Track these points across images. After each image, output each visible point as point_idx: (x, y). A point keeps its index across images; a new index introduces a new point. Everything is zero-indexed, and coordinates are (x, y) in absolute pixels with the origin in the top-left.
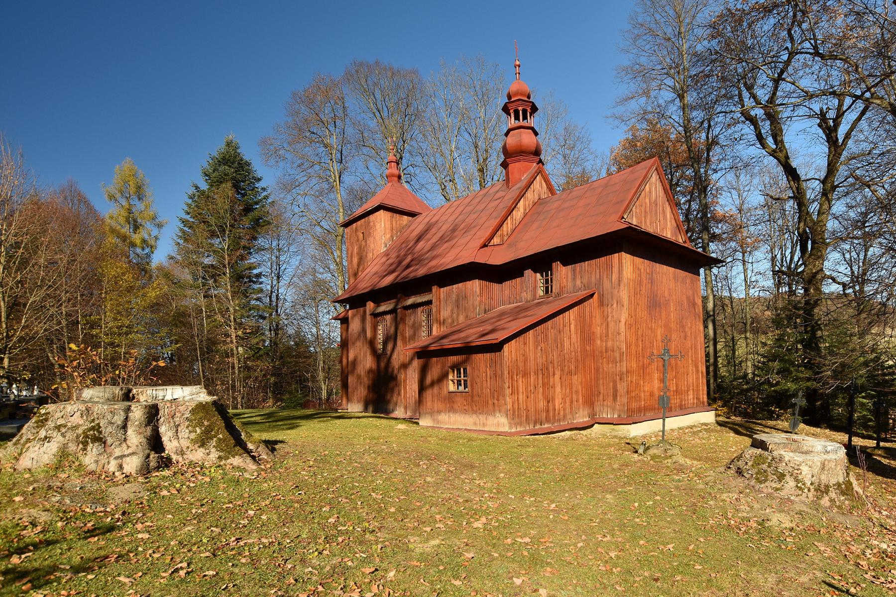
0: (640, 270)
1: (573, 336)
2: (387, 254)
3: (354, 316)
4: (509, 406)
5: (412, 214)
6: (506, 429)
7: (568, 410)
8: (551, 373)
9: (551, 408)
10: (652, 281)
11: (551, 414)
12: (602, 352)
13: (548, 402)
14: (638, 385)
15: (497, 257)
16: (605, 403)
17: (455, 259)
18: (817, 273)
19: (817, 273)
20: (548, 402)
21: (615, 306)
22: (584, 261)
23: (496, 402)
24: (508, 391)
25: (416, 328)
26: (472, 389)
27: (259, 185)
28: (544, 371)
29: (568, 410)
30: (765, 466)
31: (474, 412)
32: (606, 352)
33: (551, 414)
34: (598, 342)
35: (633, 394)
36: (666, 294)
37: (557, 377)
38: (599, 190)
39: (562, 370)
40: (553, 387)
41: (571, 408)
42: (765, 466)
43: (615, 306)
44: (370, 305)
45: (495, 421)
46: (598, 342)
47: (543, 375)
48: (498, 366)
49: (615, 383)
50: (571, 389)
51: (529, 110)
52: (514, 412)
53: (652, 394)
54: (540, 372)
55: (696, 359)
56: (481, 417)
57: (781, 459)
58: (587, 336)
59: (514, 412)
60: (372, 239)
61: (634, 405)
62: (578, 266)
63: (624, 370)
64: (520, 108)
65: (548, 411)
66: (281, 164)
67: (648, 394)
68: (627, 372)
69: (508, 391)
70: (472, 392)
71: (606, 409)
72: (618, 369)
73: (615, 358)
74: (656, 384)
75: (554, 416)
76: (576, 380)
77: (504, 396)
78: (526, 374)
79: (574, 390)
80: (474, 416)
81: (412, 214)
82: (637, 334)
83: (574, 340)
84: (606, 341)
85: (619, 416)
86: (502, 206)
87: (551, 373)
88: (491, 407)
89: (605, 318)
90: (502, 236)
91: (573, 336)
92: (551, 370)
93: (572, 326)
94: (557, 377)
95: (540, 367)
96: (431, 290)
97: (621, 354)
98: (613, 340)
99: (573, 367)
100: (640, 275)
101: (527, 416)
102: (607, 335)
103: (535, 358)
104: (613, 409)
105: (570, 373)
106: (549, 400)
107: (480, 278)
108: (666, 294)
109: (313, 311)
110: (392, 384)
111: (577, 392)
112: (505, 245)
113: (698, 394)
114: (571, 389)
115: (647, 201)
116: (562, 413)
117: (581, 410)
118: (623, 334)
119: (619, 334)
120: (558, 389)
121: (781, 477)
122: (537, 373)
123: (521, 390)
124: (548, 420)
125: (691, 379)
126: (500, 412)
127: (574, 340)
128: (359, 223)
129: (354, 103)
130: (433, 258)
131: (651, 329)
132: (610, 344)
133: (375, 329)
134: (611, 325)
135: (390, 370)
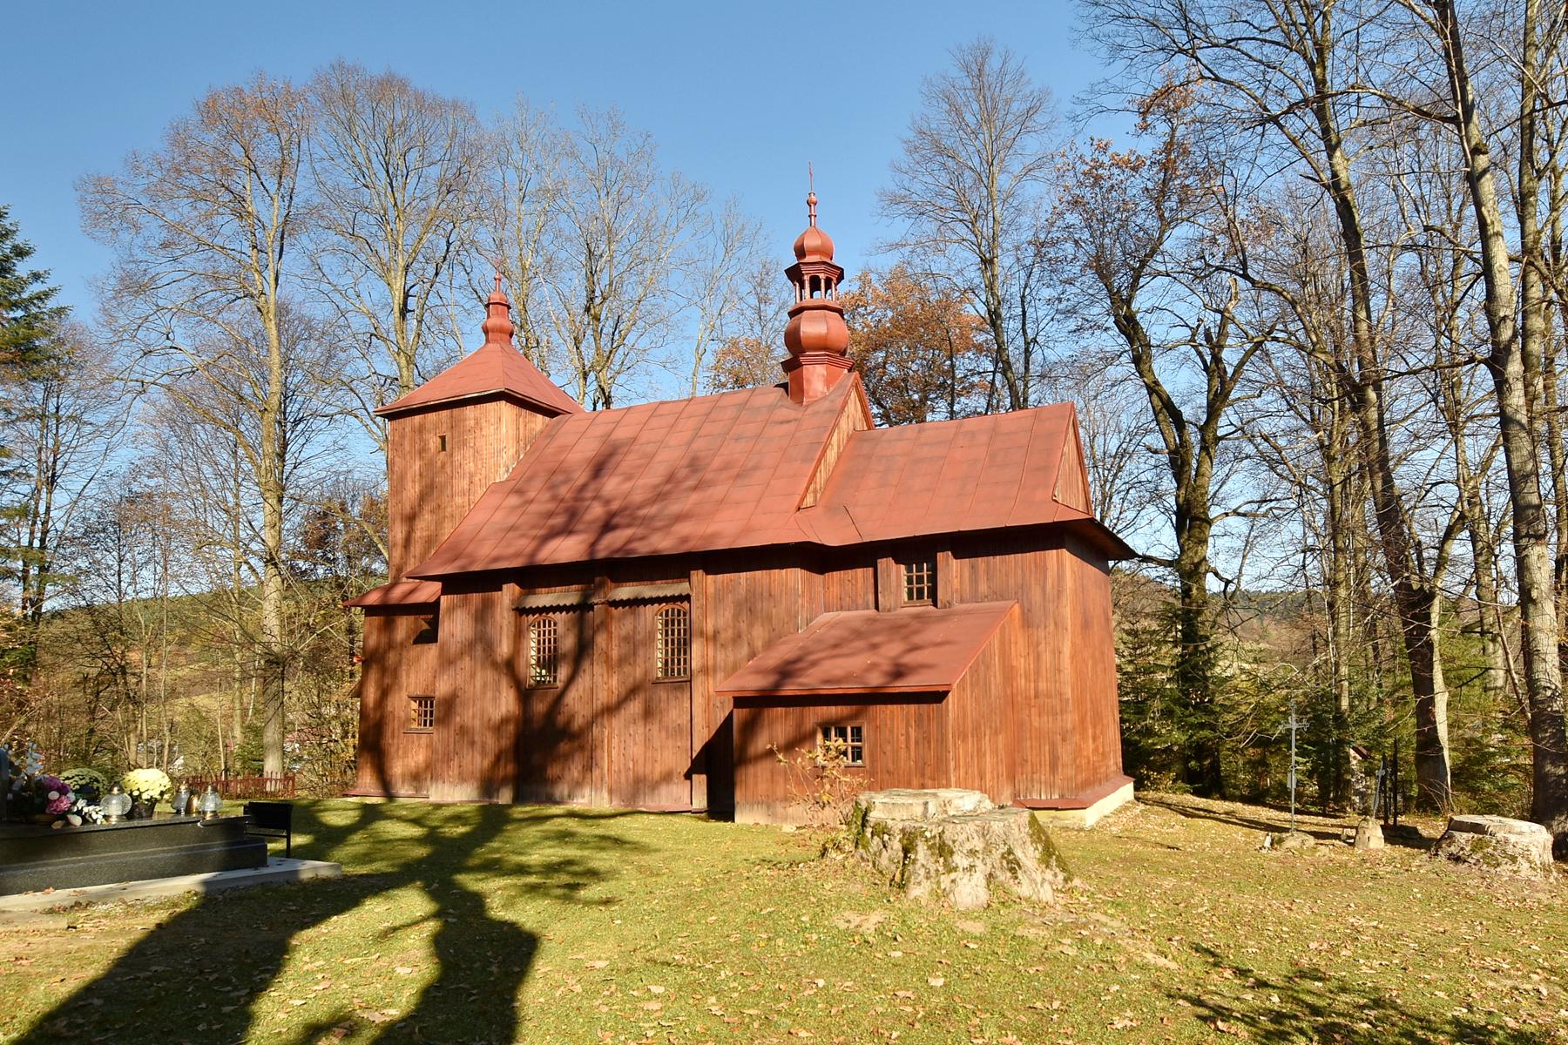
2: (517, 488)
3: (452, 609)
5: (551, 413)
15: (833, 536)
17: (747, 531)
18: (1200, 563)
19: (1200, 563)
22: (994, 554)
25: (635, 645)
26: (873, 761)
27: (22, 268)
30: (1490, 850)
32: (1036, 696)
42: (1490, 850)
43: (1052, 627)
48: (934, 725)
49: (1053, 745)
57: (1506, 841)
60: (469, 453)
62: (981, 562)
64: (822, 276)
66: (126, 237)
70: (872, 766)
71: (1037, 786)
81: (551, 413)
84: (1036, 681)
85: (1062, 796)
89: (1033, 645)
90: (815, 492)
96: (688, 577)
102: (1037, 673)
104: (1051, 786)
107: (802, 567)
109: (111, 559)
110: (564, 747)
121: (1513, 859)
128: (432, 416)
129: (321, 139)
130: (680, 518)
133: (519, 636)
135: (561, 719)
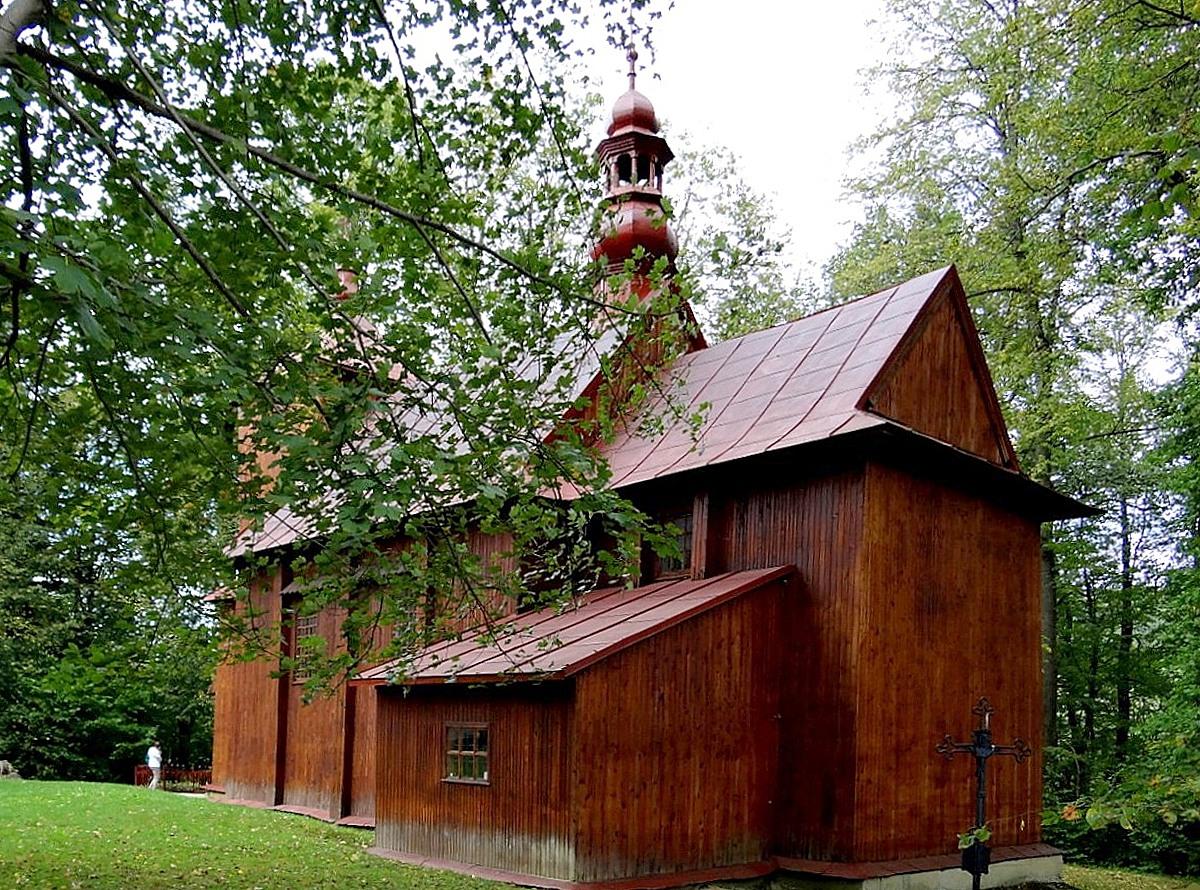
4: (582, 825)
36: (960, 583)
37: (696, 759)
39: (707, 748)
41: (723, 836)
51: (633, 154)
53: (914, 812)
65: (669, 839)
74: (926, 789)
93: (736, 649)
94: (696, 759)
100: (901, 537)
106: (675, 814)
108: (960, 583)
115: (926, 365)
131: (921, 662)
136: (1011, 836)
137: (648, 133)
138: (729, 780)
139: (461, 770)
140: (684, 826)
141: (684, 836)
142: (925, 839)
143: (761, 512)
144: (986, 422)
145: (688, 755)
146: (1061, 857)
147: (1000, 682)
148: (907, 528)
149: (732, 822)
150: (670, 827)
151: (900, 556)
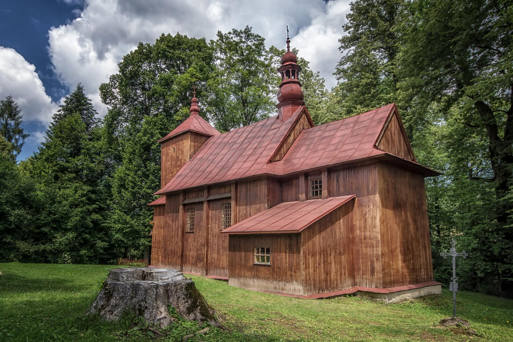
0: (387, 181)
1: (342, 227)
4: (304, 278)
6: (302, 293)
7: (339, 281)
8: (329, 254)
9: (329, 279)
10: (395, 189)
11: (329, 284)
12: (361, 239)
13: (327, 274)
14: (389, 264)
16: (365, 276)
20: (327, 274)
21: (371, 207)
23: (293, 273)
24: (302, 267)
28: (324, 252)
29: (339, 281)
31: (274, 279)
33: (329, 284)
34: (358, 232)
35: (386, 271)
36: (404, 198)
37: (332, 256)
38: (352, 125)
39: (335, 252)
40: (330, 264)
41: (341, 280)
43: (371, 207)
44: (181, 198)
45: (292, 287)
46: (358, 232)
47: (324, 255)
49: (372, 262)
50: (341, 265)
52: (306, 282)
54: (322, 253)
55: (425, 244)
56: (280, 283)
58: (351, 229)
59: (306, 282)
61: (388, 279)
63: (380, 253)
65: (327, 281)
67: (395, 271)
68: (382, 255)
69: (302, 267)
72: (375, 252)
73: (372, 244)
75: (331, 285)
76: (344, 258)
77: (300, 270)
78: (314, 255)
79: (343, 266)
80: (275, 282)
82: (387, 228)
83: (342, 230)
84: (365, 232)
86: (278, 134)
87: (329, 254)
88: (289, 277)
91: (342, 227)
92: (329, 251)
94: (332, 256)
95: (322, 249)
97: (377, 242)
98: (370, 231)
99: (342, 249)
100: (388, 185)
101: (314, 285)
102: (365, 227)
103: (320, 243)
104: (371, 281)
105: (340, 254)
106: (327, 273)
108: (404, 198)
111: (344, 267)
112: (282, 161)
113: (427, 272)
114: (341, 265)
116: (335, 283)
117: (347, 280)
118: (378, 227)
119: (375, 227)
120: (333, 266)
122: (320, 254)
123: (311, 266)
124: (327, 288)
125: (422, 260)
126: (296, 281)
127: (342, 230)
132: (368, 234)
134: (369, 220)
136: (425, 278)
137: (295, 64)
138: (340, 262)
139: (260, 260)
140: (331, 277)
141: (331, 280)
142: (401, 280)
143: (344, 178)
144: (406, 149)
145: (330, 255)
146: (440, 286)
147: (417, 228)
148: (389, 182)
149: (343, 276)
150: (327, 278)
151: (388, 191)
